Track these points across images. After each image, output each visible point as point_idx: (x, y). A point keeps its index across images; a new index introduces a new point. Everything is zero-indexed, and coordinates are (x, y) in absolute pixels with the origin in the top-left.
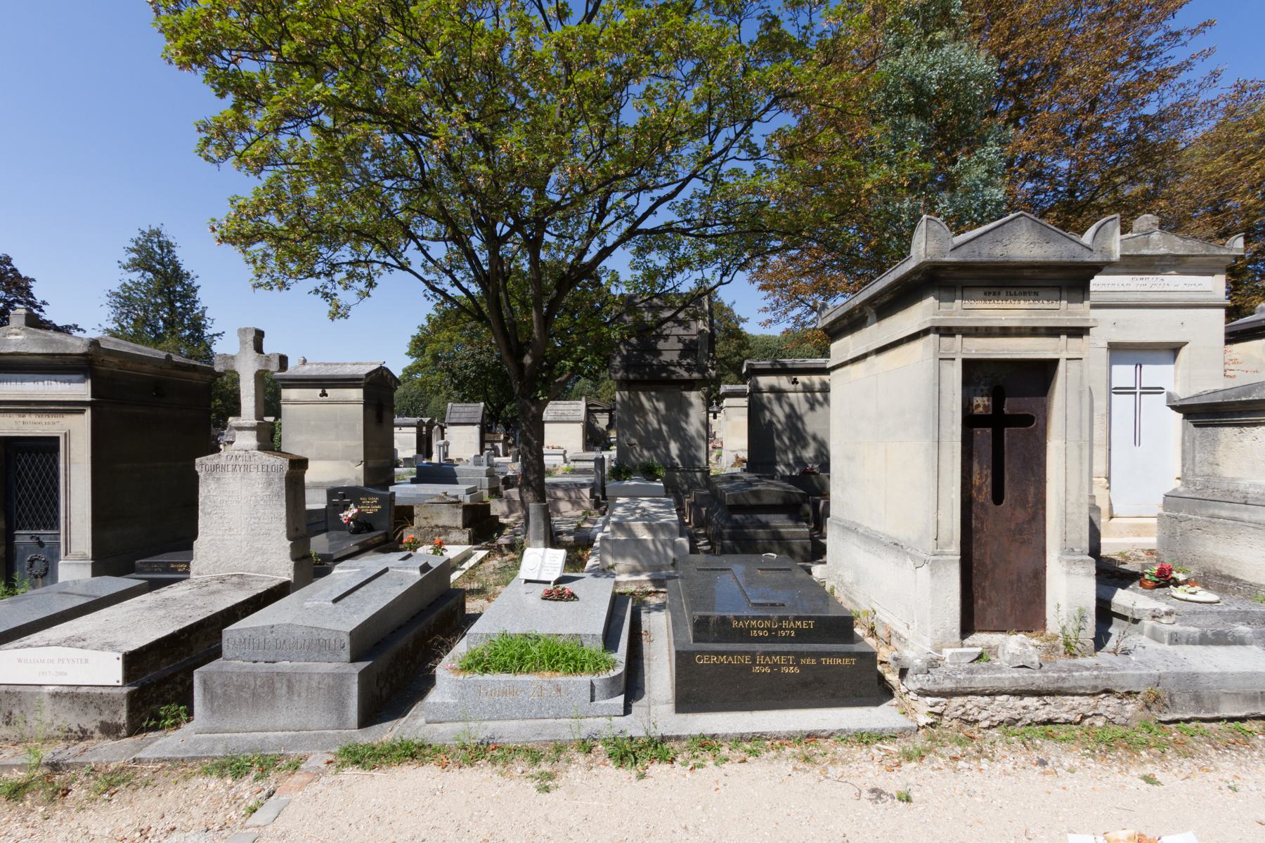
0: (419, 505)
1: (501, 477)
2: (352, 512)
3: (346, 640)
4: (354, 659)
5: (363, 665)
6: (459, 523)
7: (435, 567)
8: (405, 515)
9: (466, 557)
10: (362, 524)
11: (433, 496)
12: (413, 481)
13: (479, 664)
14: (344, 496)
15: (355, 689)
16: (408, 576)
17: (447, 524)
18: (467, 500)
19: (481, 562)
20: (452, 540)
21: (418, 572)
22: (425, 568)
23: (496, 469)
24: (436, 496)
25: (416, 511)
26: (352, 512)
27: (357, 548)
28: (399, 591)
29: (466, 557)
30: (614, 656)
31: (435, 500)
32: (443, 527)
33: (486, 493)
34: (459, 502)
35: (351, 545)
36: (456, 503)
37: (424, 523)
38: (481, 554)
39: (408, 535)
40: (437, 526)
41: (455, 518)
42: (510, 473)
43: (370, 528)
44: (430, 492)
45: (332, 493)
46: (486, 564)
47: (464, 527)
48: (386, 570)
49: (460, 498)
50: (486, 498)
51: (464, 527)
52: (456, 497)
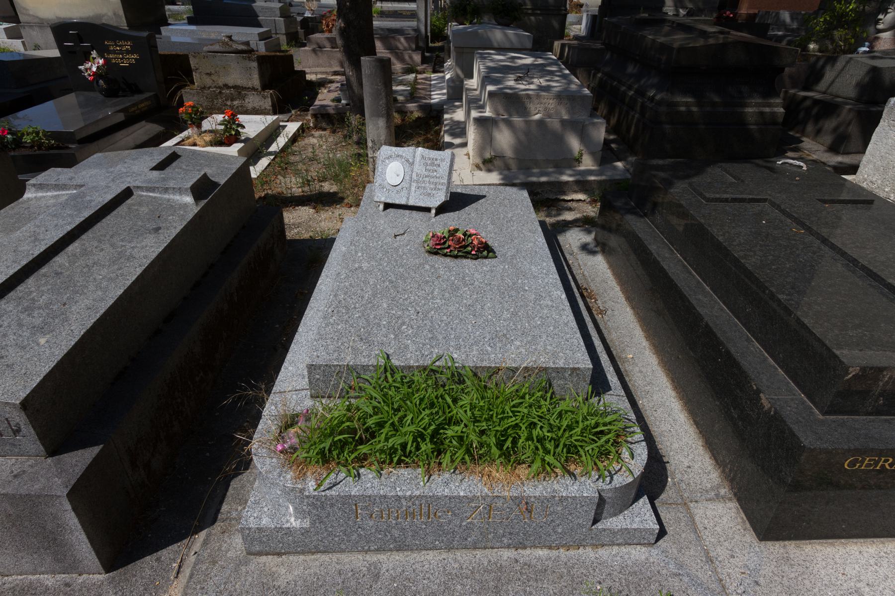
0: (197, 54)
1: (299, 19)
2: (93, 65)
3: (19, 418)
4: (54, 448)
5: (80, 460)
6: (256, 81)
7: (222, 181)
8: (178, 68)
9: (272, 133)
10: (114, 83)
11: (213, 42)
12: (191, 21)
13: (341, 444)
14: (79, 38)
15: (72, 520)
16: (172, 207)
17: (239, 82)
18: (261, 48)
19: (294, 139)
20: (250, 106)
21: (189, 199)
22: (202, 188)
23: (292, 9)
24: (218, 41)
25: (193, 63)
26: (93, 65)
27: (121, 117)
28: (151, 248)
29: (272, 133)
30: (607, 398)
31: (217, 47)
32: (235, 87)
33: (283, 39)
34: (251, 51)
35: (110, 113)
36: (247, 52)
37: (208, 81)
38: (292, 127)
39: (190, 99)
40: (226, 86)
41: (244, 74)
42: (308, 14)
43: (134, 89)
44: (213, 36)
45: (61, 30)
46: (301, 143)
47: (264, 87)
48: (127, 193)
49: (253, 45)
50: (284, 47)
51: (264, 87)
52: (247, 43)
